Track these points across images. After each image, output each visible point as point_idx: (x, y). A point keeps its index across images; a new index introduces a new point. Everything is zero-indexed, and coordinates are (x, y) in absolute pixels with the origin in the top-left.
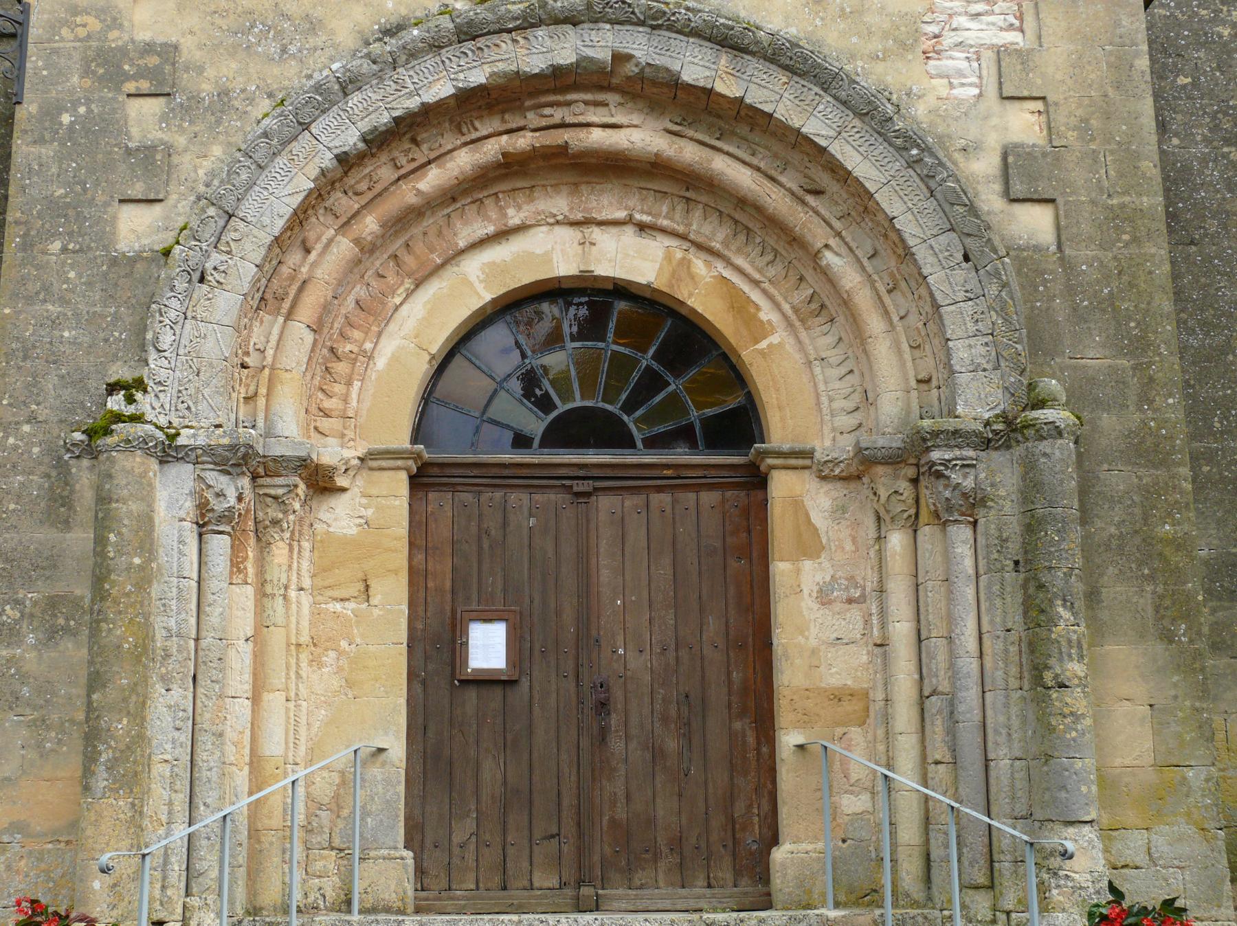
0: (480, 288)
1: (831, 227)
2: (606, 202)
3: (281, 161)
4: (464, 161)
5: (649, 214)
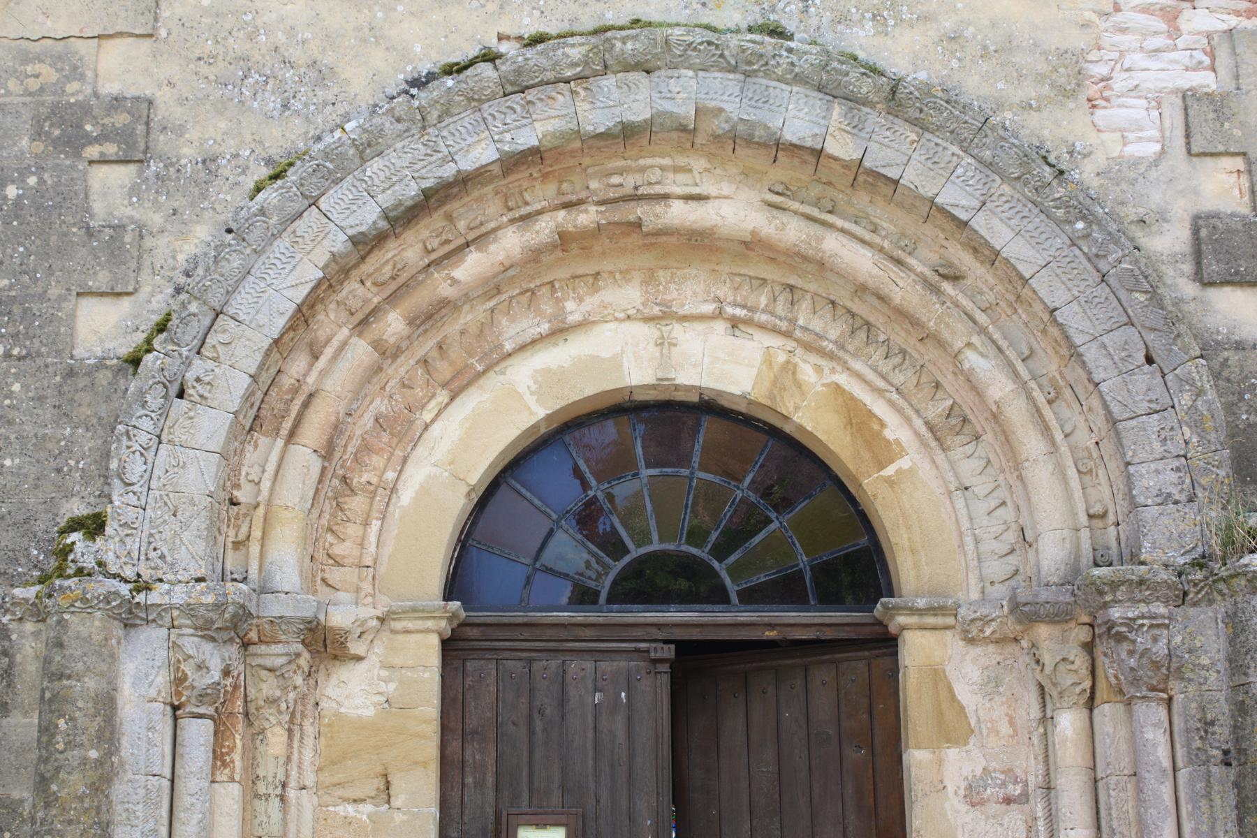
0: (531, 401)
3: (282, 244)
5: (744, 307)
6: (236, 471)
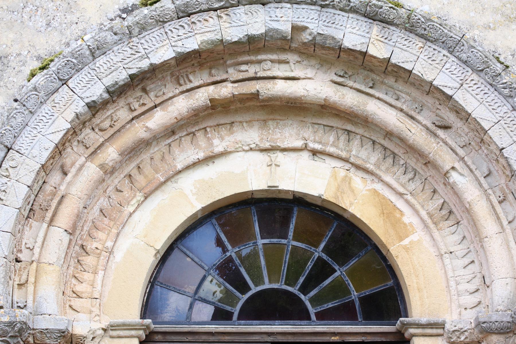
1: (457, 154)
2: (287, 134)
3: (46, 108)
4: (181, 105)
5: (320, 143)
6: (20, 242)
